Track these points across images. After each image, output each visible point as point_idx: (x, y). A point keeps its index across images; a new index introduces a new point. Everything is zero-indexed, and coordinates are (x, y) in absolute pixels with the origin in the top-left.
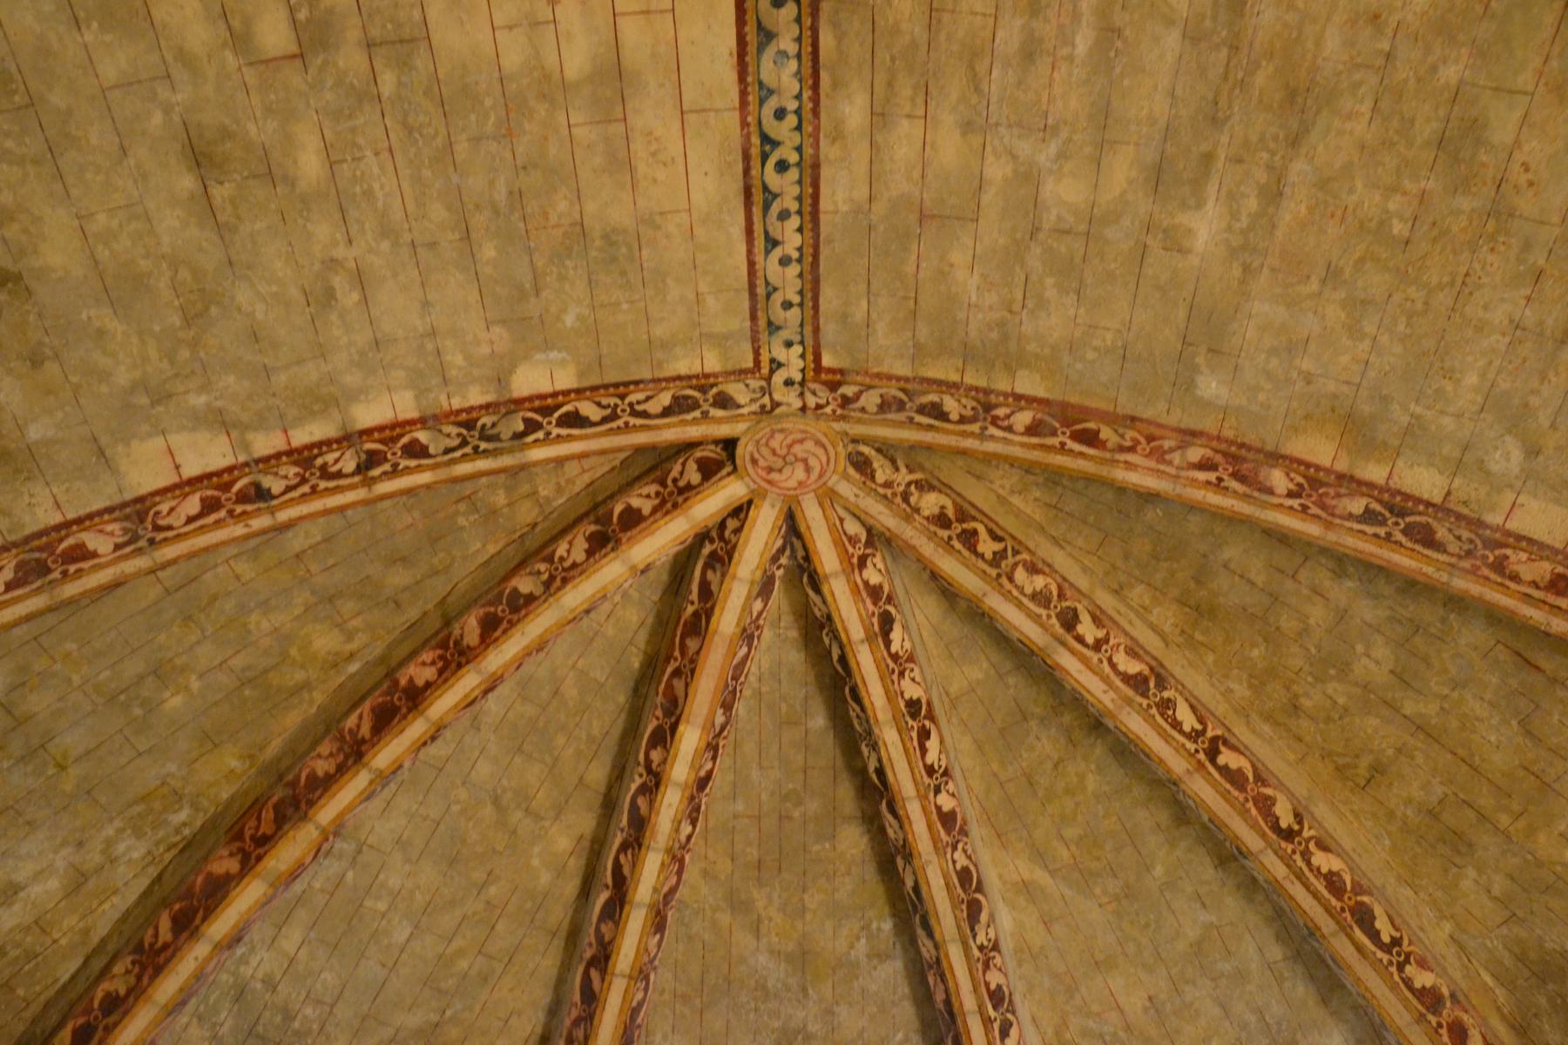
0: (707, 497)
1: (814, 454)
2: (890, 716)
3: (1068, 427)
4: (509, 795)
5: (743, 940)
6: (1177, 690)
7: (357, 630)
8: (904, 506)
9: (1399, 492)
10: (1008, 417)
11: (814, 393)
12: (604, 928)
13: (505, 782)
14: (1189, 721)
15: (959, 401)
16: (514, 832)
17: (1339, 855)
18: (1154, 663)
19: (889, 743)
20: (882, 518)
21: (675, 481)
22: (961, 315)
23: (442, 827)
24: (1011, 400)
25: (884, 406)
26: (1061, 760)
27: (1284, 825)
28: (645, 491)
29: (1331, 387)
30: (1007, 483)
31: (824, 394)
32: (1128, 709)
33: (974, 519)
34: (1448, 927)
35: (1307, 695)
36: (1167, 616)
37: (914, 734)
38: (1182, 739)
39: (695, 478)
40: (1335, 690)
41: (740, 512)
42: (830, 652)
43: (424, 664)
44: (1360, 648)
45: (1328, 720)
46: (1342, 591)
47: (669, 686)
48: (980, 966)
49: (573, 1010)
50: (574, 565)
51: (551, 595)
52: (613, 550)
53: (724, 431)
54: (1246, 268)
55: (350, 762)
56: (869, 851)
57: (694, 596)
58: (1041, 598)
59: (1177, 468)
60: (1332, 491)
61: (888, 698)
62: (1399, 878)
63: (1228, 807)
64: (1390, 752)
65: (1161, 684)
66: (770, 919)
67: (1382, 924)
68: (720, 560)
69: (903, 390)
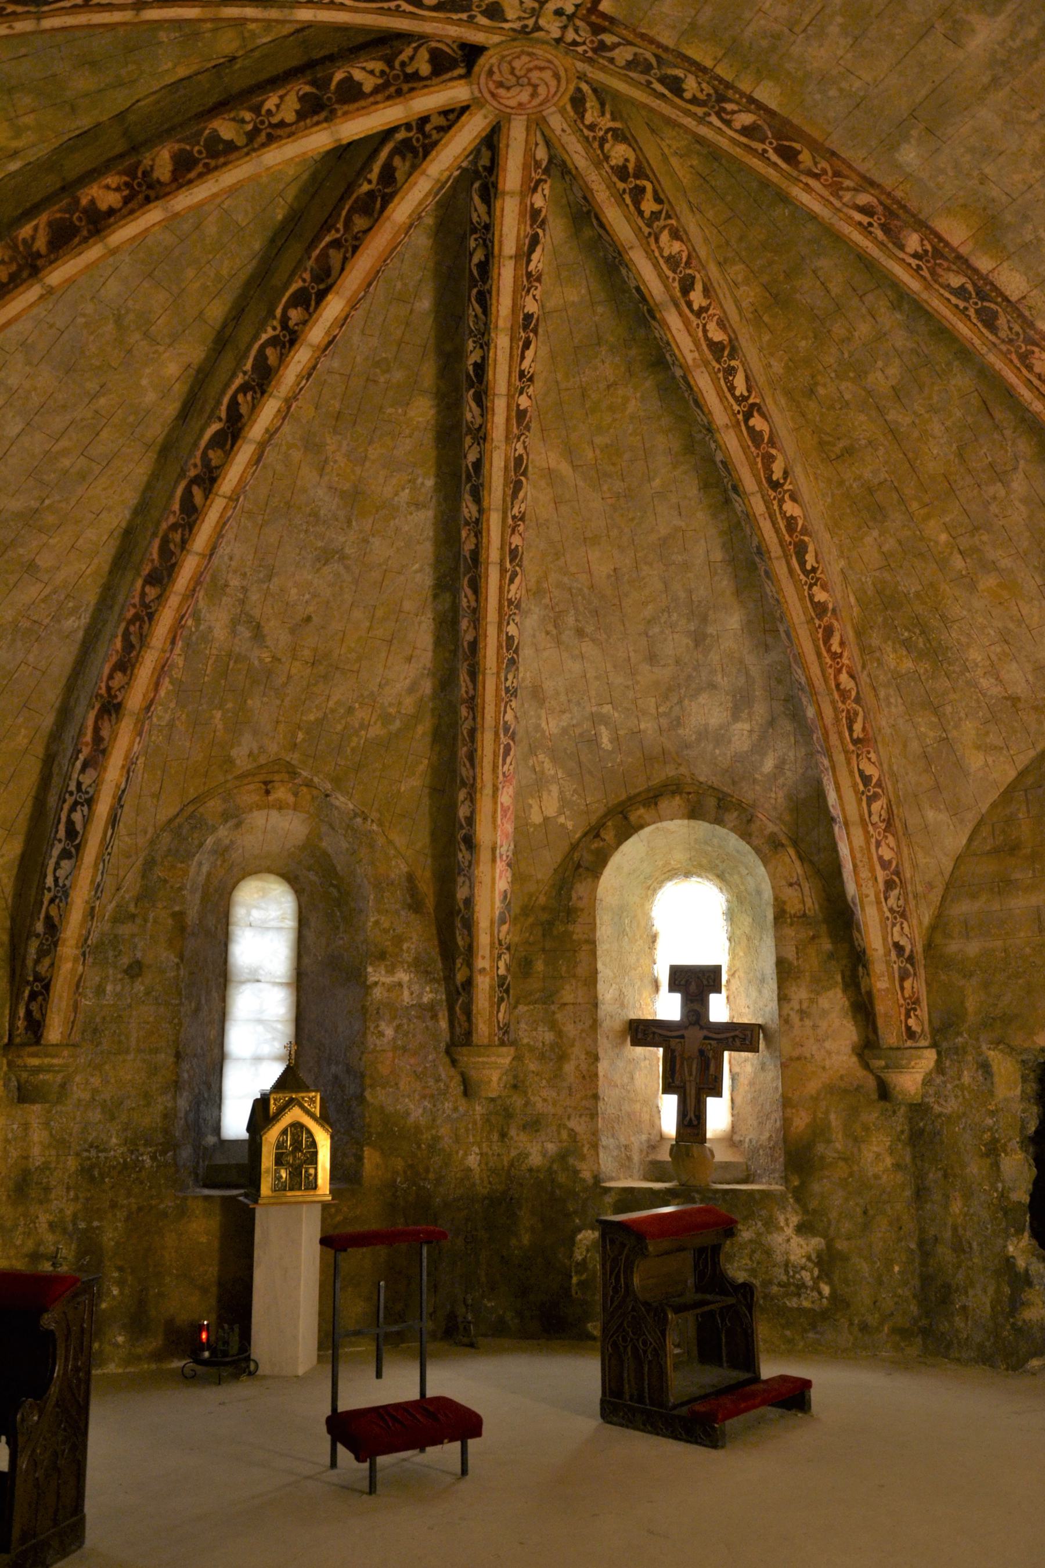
0: (432, 93)
1: (546, 84)
2: (509, 325)
3: (777, 139)
4: (131, 316)
5: (308, 475)
6: (741, 362)
7: (28, 128)
8: (599, 152)
9: (992, 284)
10: (733, 112)
11: (576, 31)
12: (211, 454)
13: (130, 303)
14: (741, 388)
15: (699, 84)
16: (130, 351)
17: (801, 506)
18: (733, 336)
19: (499, 347)
20: (575, 157)
21: (403, 64)
22: (747, 15)
23: (66, 336)
24: (744, 100)
25: (631, 65)
26: (615, 384)
27: (775, 478)
28: (371, 65)
29: (995, 192)
30: (675, 145)
31: (585, 33)
32: (704, 369)
33: (648, 179)
34: (842, 563)
35: (824, 385)
36: (749, 294)
37: (521, 344)
38: (732, 401)
39: (425, 69)
40: (848, 388)
41: (453, 115)
42: (471, 255)
43: (108, 187)
44: (880, 364)
45: (832, 407)
46: (889, 319)
47: (324, 255)
48: (510, 530)
49: (171, 516)
50: (282, 124)
51: (254, 150)
52: (326, 120)
53: (478, 37)
54: (995, 81)
55: (25, 274)
56: (433, 422)
57: (374, 175)
58: (673, 261)
59: (844, 204)
60: (945, 264)
61: (513, 311)
62: (826, 525)
63: (743, 457)
64: (863, 442)
65: (731, 356)
66: (335, 462)
67: (810, 560)
68: (414, 151)
69: (657, 57)
